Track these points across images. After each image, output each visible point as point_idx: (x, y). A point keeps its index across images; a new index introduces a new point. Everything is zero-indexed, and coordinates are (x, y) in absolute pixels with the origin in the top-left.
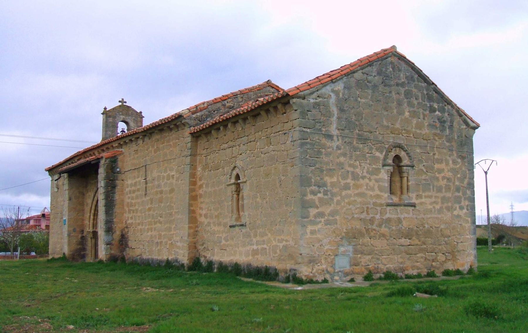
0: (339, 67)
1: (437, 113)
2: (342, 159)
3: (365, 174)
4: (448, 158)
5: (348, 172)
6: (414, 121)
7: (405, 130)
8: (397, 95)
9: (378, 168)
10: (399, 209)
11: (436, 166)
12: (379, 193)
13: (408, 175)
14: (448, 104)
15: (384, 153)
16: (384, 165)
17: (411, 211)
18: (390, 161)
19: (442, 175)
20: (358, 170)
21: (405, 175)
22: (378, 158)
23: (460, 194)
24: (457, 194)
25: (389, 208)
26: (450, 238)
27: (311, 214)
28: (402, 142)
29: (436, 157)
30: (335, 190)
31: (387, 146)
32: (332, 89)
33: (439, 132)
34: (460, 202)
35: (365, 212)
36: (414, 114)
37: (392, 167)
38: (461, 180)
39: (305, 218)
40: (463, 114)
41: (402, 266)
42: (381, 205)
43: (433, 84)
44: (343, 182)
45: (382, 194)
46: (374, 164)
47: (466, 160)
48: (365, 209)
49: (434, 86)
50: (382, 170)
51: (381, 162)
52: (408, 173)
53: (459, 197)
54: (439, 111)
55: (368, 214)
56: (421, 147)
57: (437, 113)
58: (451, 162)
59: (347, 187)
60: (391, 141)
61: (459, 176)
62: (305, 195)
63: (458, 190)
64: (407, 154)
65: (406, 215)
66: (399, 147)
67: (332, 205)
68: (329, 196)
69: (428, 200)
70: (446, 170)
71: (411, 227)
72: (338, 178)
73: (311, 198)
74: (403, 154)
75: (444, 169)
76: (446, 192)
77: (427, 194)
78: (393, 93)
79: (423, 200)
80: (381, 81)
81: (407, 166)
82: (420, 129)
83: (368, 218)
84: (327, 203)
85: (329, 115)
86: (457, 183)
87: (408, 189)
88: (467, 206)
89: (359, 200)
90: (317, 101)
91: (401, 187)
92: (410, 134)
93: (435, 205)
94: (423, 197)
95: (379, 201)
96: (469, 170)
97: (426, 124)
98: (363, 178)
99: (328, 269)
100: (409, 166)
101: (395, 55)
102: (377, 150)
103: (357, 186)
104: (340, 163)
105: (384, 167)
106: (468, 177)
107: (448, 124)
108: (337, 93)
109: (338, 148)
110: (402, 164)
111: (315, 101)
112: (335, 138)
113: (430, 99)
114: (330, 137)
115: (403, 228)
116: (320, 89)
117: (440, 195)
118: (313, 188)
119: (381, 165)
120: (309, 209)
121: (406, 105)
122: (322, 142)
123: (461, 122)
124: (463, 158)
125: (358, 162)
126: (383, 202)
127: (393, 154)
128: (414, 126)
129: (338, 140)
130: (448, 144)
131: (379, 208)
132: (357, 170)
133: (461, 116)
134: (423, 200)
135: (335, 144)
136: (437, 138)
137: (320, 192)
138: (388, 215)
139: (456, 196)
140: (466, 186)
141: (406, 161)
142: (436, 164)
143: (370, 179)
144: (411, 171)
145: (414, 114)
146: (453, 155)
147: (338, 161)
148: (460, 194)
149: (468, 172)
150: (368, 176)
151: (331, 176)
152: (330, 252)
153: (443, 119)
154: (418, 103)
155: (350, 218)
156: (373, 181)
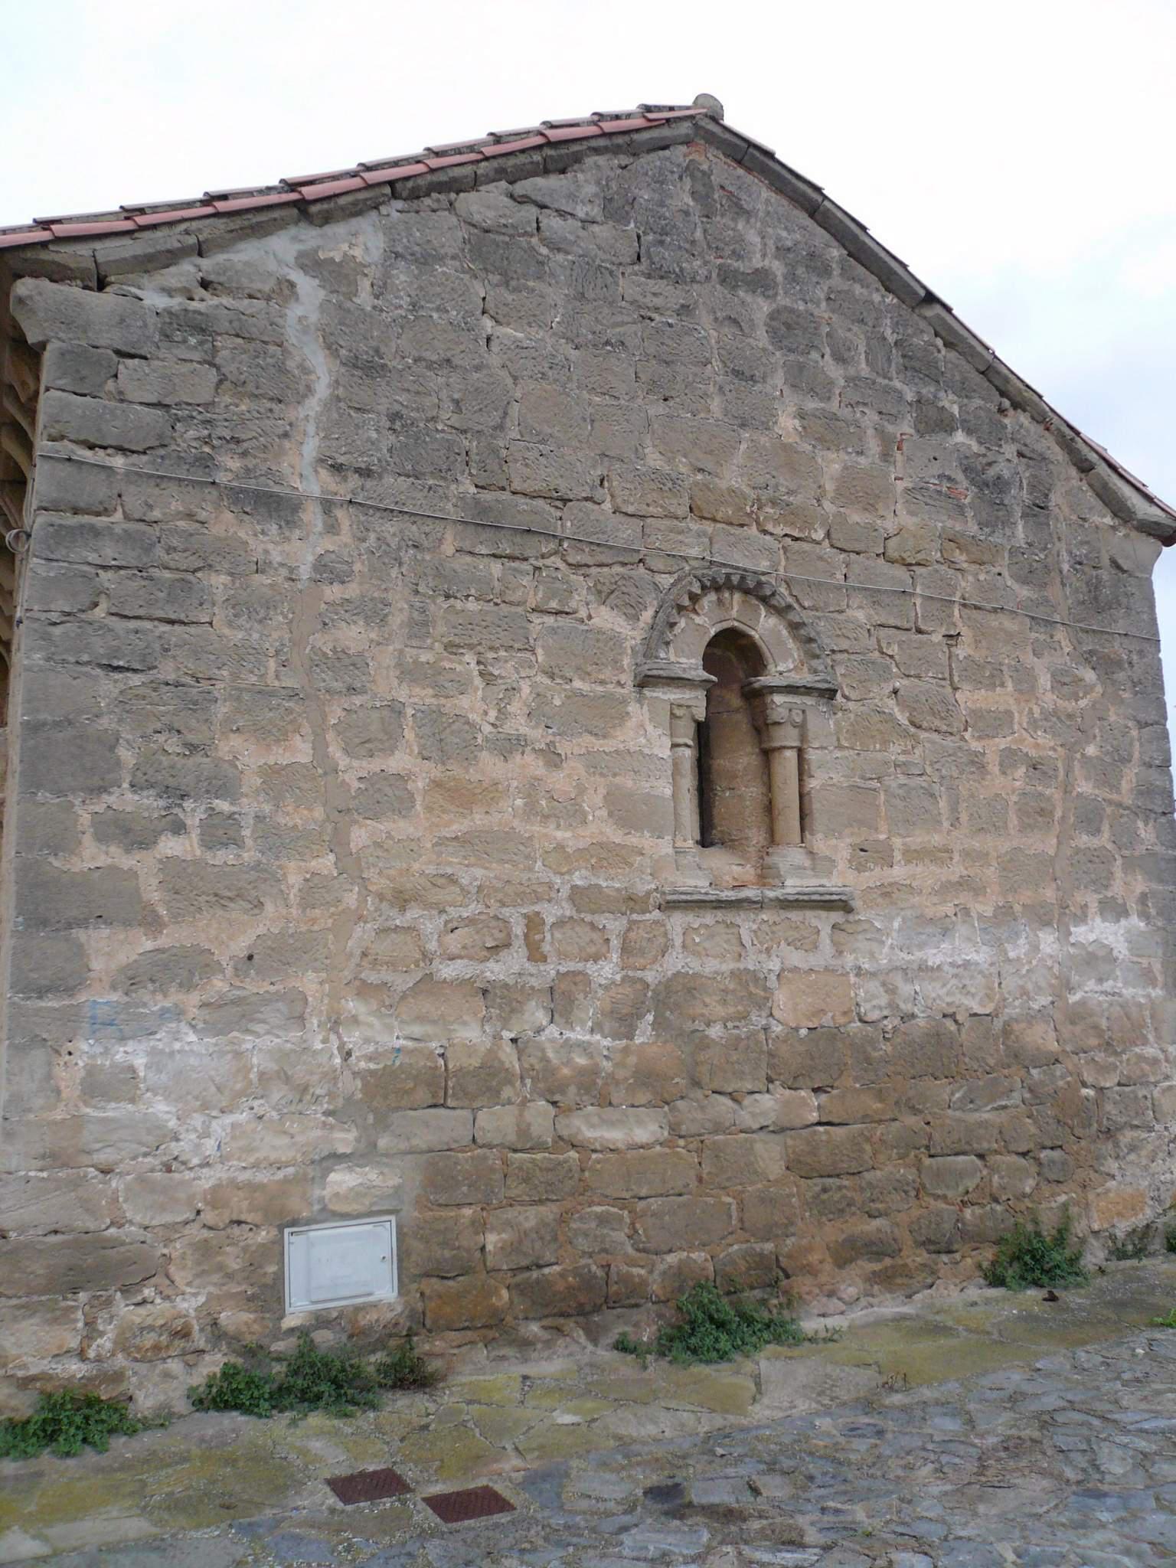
0: (352, 165)
1: (960, 437)
2: (353, 635)
3: (518, 725)
4: (1029, 659)
5: (395, 709)
6: (832, 464)
7: (774, 503)
8: (728, 330)
9: (608, 697)
10: (747, 924)
11: (969, 698)
12: (616, 836)
13: (803, 737)
14: (1016, 406)
15: (647, 616)
16: (645, 682)
17: (826, 931)
18: (688, 661)
19: (1002, 743)
20: (473, 704)
21: (786, 737)
22: (615, 640)
23: (1104, 840)
24: (1084, 840)
25: (677, 922)
26: (1058, 1070)
27: (97, 965)
28: (764, 565)
29: (961, 652)
30: (295, 817)
31: (666, 581)
32: (301, 255)
33: (973, 528)
34: (1102, 883)
35: (519, 944)
36: (827, 431)
37: (701, 694)
38: (1107, 772)
39: (41, 992)
40: (1093, 457)
41: (769, 1247)
42: (632, 902)
43: (931, 298)
44: (353, 770)
45: (633, 840)
46: (585, 675)
47: (1121, 676)
48: (519, 930)
49: (938, 309)
50: (633, 708)
51: (626, 661)
52: (802, 727)
53: (1100, 858)
54: (969, 432)
55: (536, 955)
56: (875, 597)
57: (960, 437)
58: (1045, 681)
59: (386, 796)
60: (694, 552)
61: (1091, 750)
62: (62, 842)
63: (1090, 820)
64: (795, 627)
65: (796, 958)
66: (747, 592)
67: (269, 908)
68: (249, 856)
69: (926, 875)
70: (1020, 719)
71: (826, 1020)
72: (319, 746)
73: (102, 861)
74: (765, 627)
75: (1009, 713)
76: (1024, 828)
77: (919, 839)
78: (705, 319)
79: (899, 872)
80: (627, 251)
81: (791, 689)
82: (870, 507)
83: (534, 982)
84: (239, 894)
85: (284, 387)
86: (1084, 787)
87: (803, 817)
88: (1143, 898)
89: (472, 875)
90: (195, 305)
91: (769, 809)
92: (809, 525)
93: (964, 898)
94: (898, 856)
95: (611, 883)
96: (1142, 725)
97: (900, 486)
98: (509, 746)
99: (224, 1317)
100: (807, 690)
101: (711, 139)
102: (604, 595)
103: (459, 796)
104: (341, 653)
105: (647, 692)
106: (1136, 755)
107: (1019, 497)
108: (336, 275)
109: (327, 570)
110: (764, 680)
111: (176, 303)
112: (312, 516)
113: (917, 366)
114: (274, 506)
115: (777, 1029)
116: (223, 245)
117: (990, 843)
118: (124, 800)
119: (627, 678)
120: (80, 934)
121: (779, 379)
122: (217, 530)
123: (1090, 497)
124: (1106, 665)
125: (470, 658)
126: (644, 885)
127: (707, 621)
128: (830, 486)
129: (332, 528)
130: (1025, 592)
131: (614, 925)
132: (464, 702)
133: (1084, 467)
134: (899, 872)
135: (302, 549)
136: (960, 558)
137: (179, 828)
138: (675, 962)
139: (1078, 851)
140: (1128, 801)
141: (784, 666)
142: (966, 686)
143: (552, 757)
144: (822, 724)
145: (827, 431)
146: (1054, 647)
147: (323, 642)
148: (1104, 840)
149: (1134, 733)
150: (537, 735)
151: (269, 734)
152: (239, 1205)
153: (992, 472)
154: (853, 381)
155: (402, 982)
156: (574, 768)
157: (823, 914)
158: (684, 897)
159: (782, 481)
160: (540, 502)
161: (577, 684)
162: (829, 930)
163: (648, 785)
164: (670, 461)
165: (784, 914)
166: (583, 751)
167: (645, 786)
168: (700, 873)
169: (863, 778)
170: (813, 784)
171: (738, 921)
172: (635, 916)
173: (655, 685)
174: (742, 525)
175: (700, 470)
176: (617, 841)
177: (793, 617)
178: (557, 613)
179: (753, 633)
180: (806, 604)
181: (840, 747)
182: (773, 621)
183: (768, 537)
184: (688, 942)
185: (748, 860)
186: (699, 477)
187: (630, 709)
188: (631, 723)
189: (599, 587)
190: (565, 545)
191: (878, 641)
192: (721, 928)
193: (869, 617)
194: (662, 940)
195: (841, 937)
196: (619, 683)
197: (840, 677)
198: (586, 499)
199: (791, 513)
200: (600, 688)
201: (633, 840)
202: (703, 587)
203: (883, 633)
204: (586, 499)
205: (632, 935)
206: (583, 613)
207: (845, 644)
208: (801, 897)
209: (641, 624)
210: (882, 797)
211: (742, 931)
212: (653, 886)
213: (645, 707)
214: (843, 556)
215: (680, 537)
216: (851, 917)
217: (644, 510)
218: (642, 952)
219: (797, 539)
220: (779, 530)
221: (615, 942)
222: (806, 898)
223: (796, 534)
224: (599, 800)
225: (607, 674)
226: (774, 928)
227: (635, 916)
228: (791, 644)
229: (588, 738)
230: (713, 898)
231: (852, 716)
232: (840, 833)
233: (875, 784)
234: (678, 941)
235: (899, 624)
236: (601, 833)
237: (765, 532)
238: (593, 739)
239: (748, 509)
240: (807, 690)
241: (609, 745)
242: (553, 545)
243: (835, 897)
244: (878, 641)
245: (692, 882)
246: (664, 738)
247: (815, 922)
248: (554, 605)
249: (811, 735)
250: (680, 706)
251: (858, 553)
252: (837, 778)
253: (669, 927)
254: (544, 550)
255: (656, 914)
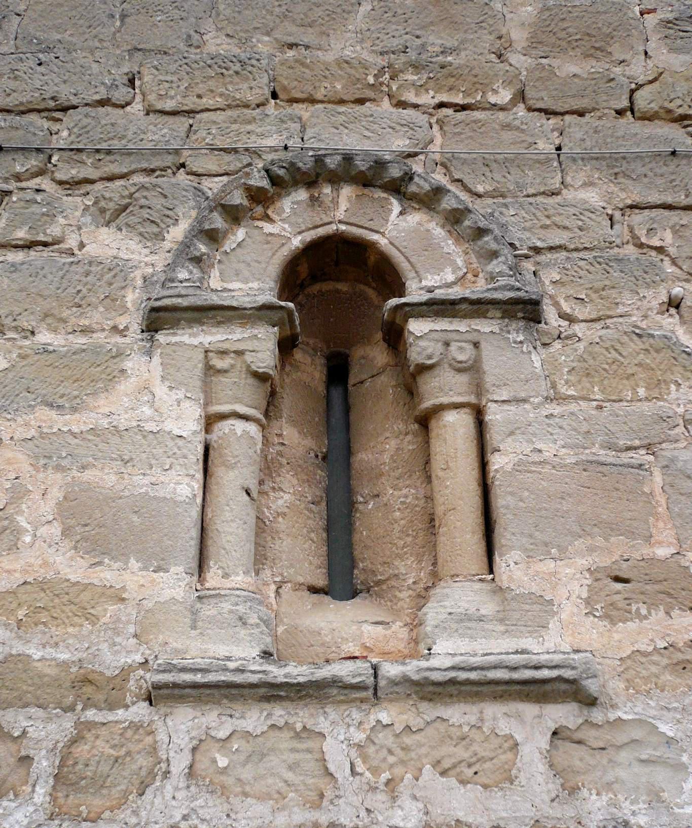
7: (416, 67)
10: (339, 733)
12: (71, 567)
13: (479, 388)
16: (158, 319)
25: (181, 726)
42: (89, 687)
45: (107, 575)
50: (134, 363)
52: (473, 369)
64: (455, 218)
74: (396, 229)
92: (485, 86)
100: (477, 307)
102: (113, 215)
105: (161, 337)
126: (115, 656)
127: (291, 226)
128: (519, 36)
131: (45, 731)
144: (506, 355)
157: (529, 710)
158: (188, 677)
159: (432, 39)
160: (33, 117)
161: (44, 337)
162: (544, 742)
163: (146, 480)
164: (242, 43)
165: (430, 711)
166: (32, 433)
167: (140, 483)
168: (243, 632)
169: (610, 446)
170: (497, 462)
171: (323, 724)
172: (91, 714)
173: (174, 324)
174: (361, 101)
175: (291, 46)
176: (73, 578)
177: (448, 203)
178: (29, 245)
179: (375, 237)
180: (480, 189)
181: (557, 398)
182: (415, 218)
183: (410, 112)
184: (203, 764)
185: (397, 613)
186: (290, 53)
187: (128, 365)
188: (125, 386)
189: (103, 204)
190: (54, 159)
191: (631, 230)
192: (284, 741)
193: (609, 197)
194: (143, 762)
195: (573, 756)
196: (115, 329)
197: (548, 281)
198: (102, 103)
199: (442, 73)
200: (81, 341)
201: (107, 575)
202: (275, 180)
203: (638, 218)
204: (102, 103)
205: (81, 750)
206: (72, 242)
207: (557, 237)
208: (463, 676)
209: (167, 245)
210: (658, 478)
211: (329, 746)
212: (139, 658)
213: (156, 360)
214: (553, 121)
215: (249, 127)
216: (597, 715)
217: (191, 103)
218: (99, 784)
219: (464, 108)
220: (428, 99)
221: (44, 764)
222: (473, 676)
223: (459, 99)
224: (47, 508)
225: (95, 317)
226: (408, 740)
227: (91, 714)
228: (450, 246)
229: (45, 414)
230: (254, 679)
231: (581, 346)
232: (562, 549)
233: (641, 456)
234: (180, 764)
235: (669, 200)
236: (45, 564)
237: (402, 105)
238: (53, 414)
239: (371, 80)
240: (477, 307)
241: (78, 423)
242: (34, 162)
243: (545, 673)
244: (631, 230)
245: (222, 650)
246: (187, 404)
247: (505, 727)
248: (21, 234)
249: (489, 379)
250: (223, 353)
251: (581, 114)
252: (549, 450)
253: (162, 736)
254: (18, 168)
255: (140, 711)
